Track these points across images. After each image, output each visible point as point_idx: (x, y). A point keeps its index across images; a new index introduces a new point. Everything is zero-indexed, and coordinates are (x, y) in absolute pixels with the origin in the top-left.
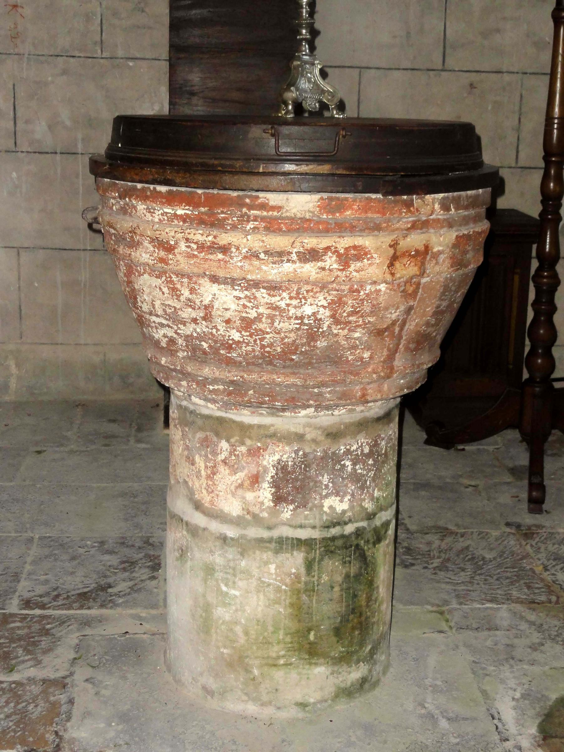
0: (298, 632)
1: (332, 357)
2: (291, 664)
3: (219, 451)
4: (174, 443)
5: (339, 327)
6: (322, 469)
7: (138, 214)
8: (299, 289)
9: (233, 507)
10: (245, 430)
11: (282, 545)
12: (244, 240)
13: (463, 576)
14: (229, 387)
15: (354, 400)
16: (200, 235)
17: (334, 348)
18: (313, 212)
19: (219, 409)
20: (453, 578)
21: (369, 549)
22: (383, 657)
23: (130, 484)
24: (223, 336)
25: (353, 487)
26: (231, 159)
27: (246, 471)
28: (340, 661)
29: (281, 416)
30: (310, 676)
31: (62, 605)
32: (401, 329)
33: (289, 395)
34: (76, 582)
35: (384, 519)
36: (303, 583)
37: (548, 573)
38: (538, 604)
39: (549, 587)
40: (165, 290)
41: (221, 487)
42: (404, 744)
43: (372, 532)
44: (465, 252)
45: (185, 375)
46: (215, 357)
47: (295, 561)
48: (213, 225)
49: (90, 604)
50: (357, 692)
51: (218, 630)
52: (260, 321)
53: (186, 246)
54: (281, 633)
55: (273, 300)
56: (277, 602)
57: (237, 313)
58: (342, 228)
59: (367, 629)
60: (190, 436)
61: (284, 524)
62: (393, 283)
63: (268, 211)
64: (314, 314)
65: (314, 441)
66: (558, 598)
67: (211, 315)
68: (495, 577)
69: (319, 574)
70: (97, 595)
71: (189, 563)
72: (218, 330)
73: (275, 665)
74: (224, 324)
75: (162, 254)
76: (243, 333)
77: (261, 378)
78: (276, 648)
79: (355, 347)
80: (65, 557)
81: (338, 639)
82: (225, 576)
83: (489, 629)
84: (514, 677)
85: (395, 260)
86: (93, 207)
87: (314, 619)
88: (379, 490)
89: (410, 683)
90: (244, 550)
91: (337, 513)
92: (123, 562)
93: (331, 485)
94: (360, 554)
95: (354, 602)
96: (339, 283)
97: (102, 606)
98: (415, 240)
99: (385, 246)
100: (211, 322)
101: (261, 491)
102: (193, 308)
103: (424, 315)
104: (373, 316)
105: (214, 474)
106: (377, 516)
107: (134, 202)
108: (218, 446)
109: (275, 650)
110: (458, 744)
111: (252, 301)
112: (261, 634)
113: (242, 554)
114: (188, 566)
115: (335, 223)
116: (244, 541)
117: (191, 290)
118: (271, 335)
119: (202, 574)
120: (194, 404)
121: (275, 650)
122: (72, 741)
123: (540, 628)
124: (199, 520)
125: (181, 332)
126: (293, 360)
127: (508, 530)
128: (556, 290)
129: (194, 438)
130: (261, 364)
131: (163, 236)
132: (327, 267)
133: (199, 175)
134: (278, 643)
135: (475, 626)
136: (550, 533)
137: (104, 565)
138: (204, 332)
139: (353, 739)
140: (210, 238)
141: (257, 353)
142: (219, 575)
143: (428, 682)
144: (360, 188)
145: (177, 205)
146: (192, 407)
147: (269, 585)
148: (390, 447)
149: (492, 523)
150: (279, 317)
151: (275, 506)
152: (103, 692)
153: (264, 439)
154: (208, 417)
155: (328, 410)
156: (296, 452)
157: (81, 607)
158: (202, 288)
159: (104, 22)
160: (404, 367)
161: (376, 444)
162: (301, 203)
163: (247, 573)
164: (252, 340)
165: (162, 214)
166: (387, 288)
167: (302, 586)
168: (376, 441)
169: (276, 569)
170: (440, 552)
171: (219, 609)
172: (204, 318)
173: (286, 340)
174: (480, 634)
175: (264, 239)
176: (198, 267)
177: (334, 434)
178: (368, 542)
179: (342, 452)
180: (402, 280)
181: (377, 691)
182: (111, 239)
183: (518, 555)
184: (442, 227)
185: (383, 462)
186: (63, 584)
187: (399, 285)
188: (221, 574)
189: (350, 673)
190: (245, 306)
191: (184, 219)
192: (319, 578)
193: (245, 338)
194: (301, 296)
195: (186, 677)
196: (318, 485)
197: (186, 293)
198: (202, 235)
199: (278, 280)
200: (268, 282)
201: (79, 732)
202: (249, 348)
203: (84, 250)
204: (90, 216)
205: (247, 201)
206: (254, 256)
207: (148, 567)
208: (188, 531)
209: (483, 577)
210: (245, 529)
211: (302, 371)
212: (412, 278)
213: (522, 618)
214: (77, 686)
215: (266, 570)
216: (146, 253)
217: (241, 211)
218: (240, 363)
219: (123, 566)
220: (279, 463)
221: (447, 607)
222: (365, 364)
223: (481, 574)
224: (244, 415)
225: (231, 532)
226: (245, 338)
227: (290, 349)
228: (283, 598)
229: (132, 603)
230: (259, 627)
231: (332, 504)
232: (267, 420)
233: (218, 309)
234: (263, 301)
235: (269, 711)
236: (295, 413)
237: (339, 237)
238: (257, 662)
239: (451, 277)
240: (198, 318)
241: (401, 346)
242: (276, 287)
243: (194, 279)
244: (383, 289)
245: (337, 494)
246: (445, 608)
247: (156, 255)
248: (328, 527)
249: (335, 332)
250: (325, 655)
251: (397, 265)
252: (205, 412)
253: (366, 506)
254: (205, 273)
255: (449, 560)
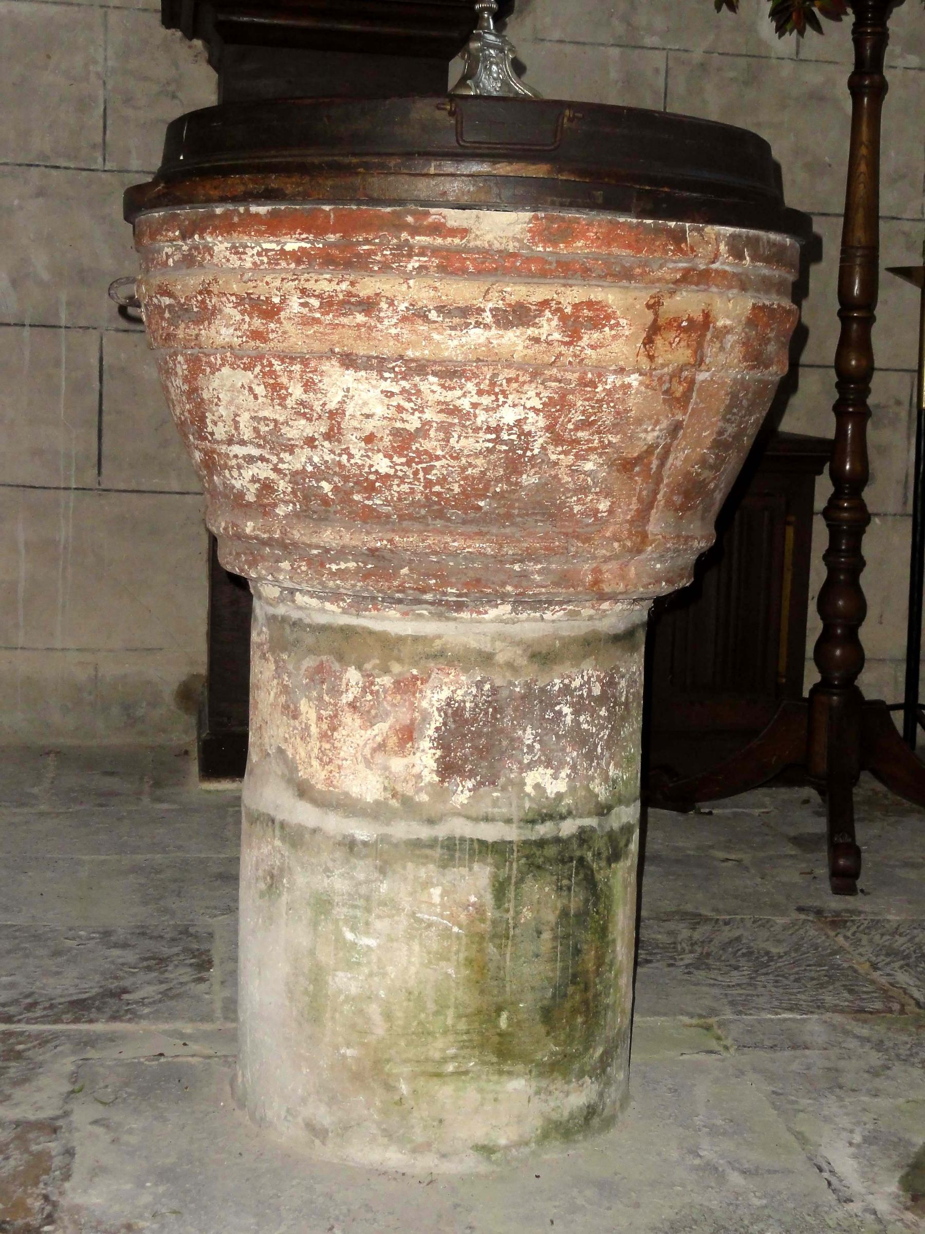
0: (479, 1012)
1: (547, 507)
2: (466, 1073)
3: (343, 687)
4: (258, 688)
5: (560, 449)
6: (523, 716)
7: (215, 261)
8: (495, 375)
9: (366, 786)
10: (389, 646)
11: (454, 851)
12: (404, 290)
13: (735, 977)
14: (366, 564)
15: (580, 589)
16: (326, 283)
17: (550, 486)
18: (520, 241)
19: (345, 611)
20: (720, 978)
21: (601, 868)
22: (621, 1076)
23: (149, 856)
24: (359, 467)
25: (575, 754)
26: (379, 154)
27: (391, 720)
28: (552, 1071)
29: (455, 619)
30: (500, 1096)
31: (42, 1017)
32: (662, 465)
33: (471, 574)
34: (65, 984)
35: (624, 820)
36: (488, 923)
37: (879, 973)
38: (871, 1013)
39: (885, 991)
40: (260, 390)
41: (346, 751)
42: (671, 1207)
43: (606, 838)
44: (765, 341)
45: (288, 548)
46: (342, 509)
47: (475, 882)
48: (348, 265)
49: (92, 1016)
50: (579, 1132)
51: (337, 1015)
52: (426, 436)
53: (302, 305)
54: (451, 1013)
55: (450, 395)
56: (443, 956)
57: (385, 422)
58: (568, 271)
59: (597, 1014)
60: (290, 667)
61: (457, 814)
62: (651, 375)
63: (445, 237)
64: (519, 423)
65: (510, 666)
66: (903, 1006)
67: (339, 428)
68: (792, 978)
69: (516, 907)
70: (104, 1003)
71: (285, 898)
72: (351, 456)
73: (438, 1075)
74: (363, 444)
75: (257, 323)
76: (395, 459)
77: (423, 541)
78: (440, 1043)
79: (583, 490)
80: (41, 952)
81: (547, 1028)
82: (351, 912)
83: (795, 1047)
84: (847, 1114)
85: (655, 333)
86: (128, 278)
87: (508, 989)
88: (616, 766)
89: (668, 1121)
90: (386, 862)
91: (547, 798)
92: (146, 959)
93: (537, 746)
94: (586, 875)
95: (576, 964)
96: (563, 368)
97: (114, 1018)
98: (686, 303)
99: (640, 306)
100: (339, 441)
101: (418, 754)
102: (308, 419)
103: (698, 442)
104: (617, 434)
105: (334, 729)
106: (613, 811)
107: (209, 239)
108: (341, 679)
109: (439, 1047)
110: (766, 1207)
111: (413, 398)
112: (415, 1017)
113: (382, 871)
114: (284, 903)
115: (558, 262)
116: (386, 847)
117: (305, 385)
118: (443, 462)
119: (307, 913)
120: (300, 608)
121: (439, 1047)
122: (76, 1209)
123: (879, 1046)
124: (304, 814)
125: (285, 466)
126: (480, 508)
127: (803, 917)
128: (864, 532)
129: (298, 668)
130: (424, 517)
131: (260, 291)
132: (543, 338)
133: (327, 178)
134: (445, 1033)
135: (767, 1043)
136: (872, 920)
137: (113, 962)
138: (326, 462)
139: (580, 1201)
140: (344, 286)
141: (418, 497)
142: (340, 912)
143: (698, 1121)
144: (600, 201)
145: (286, 234)
146: (295, 615)
147: (430, 925)
148: (633, 694)
149: (776, 908)
150: (458, 428)
151: (442, 781)
152: (125, 1138)
153: (423, 662)
154: (323, 629)
155: (535, 610)
156: (479, 685)
157: (76, 1020)
158: (326, 380)
159: (108, 112)
160: (664, 537)
161: (612, 684)
162: (502, 227)
163: (391, 905)
164: (410, 473)
165: (259, 254)
166: (641, 383)
167: (486, 927)
168: (612, 677)
169: (442, 896)
170: (692, 945)
171: (340, 974)
172: (328, 436)
173: (470, 471)
174: (779, 1054)
175: (438, 284)
176: (320, 340)
177: (544, 656)
178: (598, 855)
179: (556, 688)
180: (666, 370)
181: (612, 1134)
182: (163, 318)
183: (824, 949)
184: (730, 287)
185: (623, 719)
186: (43, 988)
187: (660, 379)
188: (345, 910)
189: (567, 1094)
190: (400, 409)
191: (298, 257)
192: (518, 913)
193: (398, 468)
194: (497, 390)
195: (275, 1110)
196: (516, 745)
197: (297, 391)
198: (330, 281)
199: (459, 359)
200: (441, 362)
201: (90, 1197)
202: (405, 488)
203: (65, 489)
204: (122, 293)
205: (410, 219)
206: (419, 317)
207: (191, 965)
208: (283, 839)
209: (771, 977)
210: (388, 824)
211: (494, 530)
212: (681, 369)
213: (846, 1033)
214: (78, 1130)
215: (424, 898)
216: (227, 326)
217: (398, 238)
218: (388, 516)
219: (145, 964)
220: (448, 705)
221: (717, 1019)
222: (601, 523)
223: (767, 974)
224: (388, 619)
225: (362, 831)
226: (398, 468)
227: (477, 487)
228: (454, 949)
229: (166, 1015)
230: (411, 1004)
231: (540, 780)
232: (429, 627)
233: (353, 416)
234: (432, 398)
235: (426, 1163)
236: (479, 613)
237: (564, 285)
238: (406, 1069)
239: (743, 378)
240: (316, 436)
241: (659, 497)
242: (456, 372)
243: (312, 364)
244: (635, 384)
245: (548, 765)
246: (712, 1020)
247: (246, 326)
248: (533, 822)
249: (553, 457)
250: (524, 1058)
251: (659, 341)
252: (322, 619)
253: (596, 790)
254: (332, 351)
255: (708, 955)
